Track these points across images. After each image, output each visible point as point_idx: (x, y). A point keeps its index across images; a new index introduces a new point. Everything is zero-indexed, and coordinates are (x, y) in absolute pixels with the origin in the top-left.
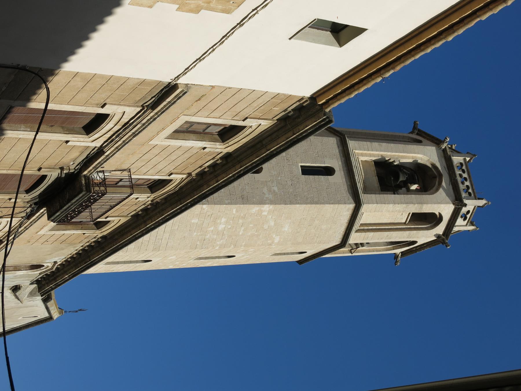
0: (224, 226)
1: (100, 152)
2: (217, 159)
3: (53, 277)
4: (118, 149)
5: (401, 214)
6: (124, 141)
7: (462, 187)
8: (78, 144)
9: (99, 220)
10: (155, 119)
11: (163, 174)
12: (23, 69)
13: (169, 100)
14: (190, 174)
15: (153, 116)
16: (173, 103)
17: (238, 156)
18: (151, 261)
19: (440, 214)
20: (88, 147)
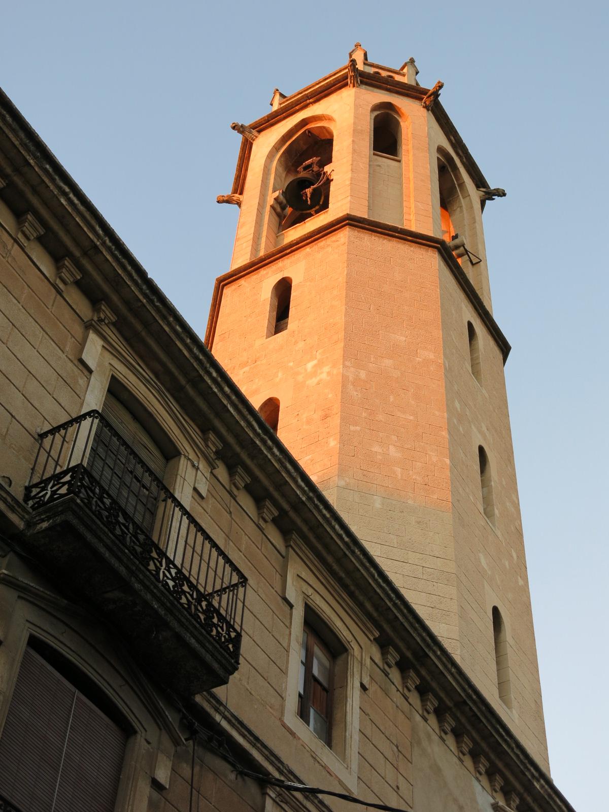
2: (460, 753)
3: (188, 387)
5: (378, 168)
17: (379, 627)
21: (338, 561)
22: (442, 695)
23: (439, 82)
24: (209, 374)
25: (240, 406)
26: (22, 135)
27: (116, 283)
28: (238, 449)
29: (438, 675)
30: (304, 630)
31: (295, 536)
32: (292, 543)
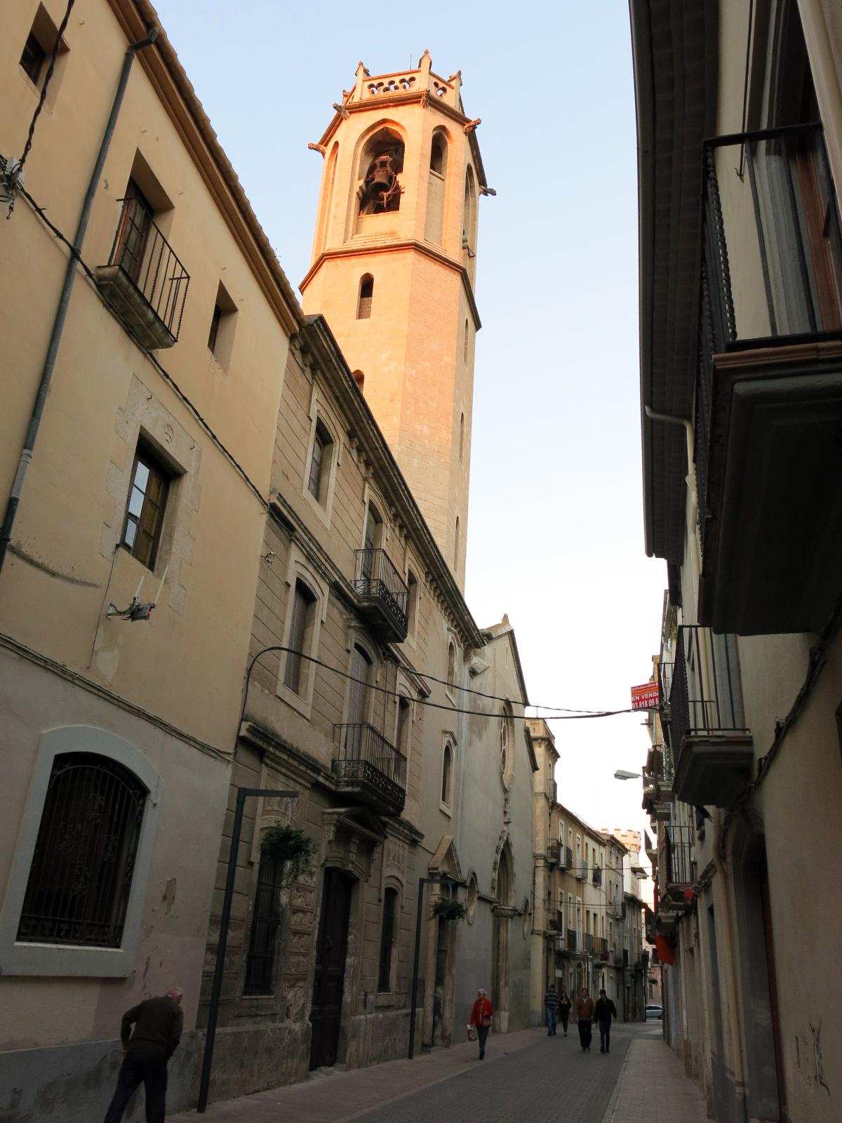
0: (425, 426)
1: (336, 588)
4: (334, 567)
6: (326, 561)
7: (401, 92)
8: (325, 610)
9: (406, 584)
10: (306, 528)
11: (363, 511)
12: (249, 671)
13: (286, 513)
14: (365, 480)
15: (302, 529)
16: (290, 508)
17: (351, 424)
18: (458, 517)
19: (435, 129)
20: (329, 599)
21: (423, 547)
22: (363, 440)
23: (479, 119)
24: (401, 488)
25: (409, 498)
26: (364, 411)
27: (379, 459)
28: (401, 512)
29: (444, 583)
30: (316, 439)
31: (410, 540)
32: (316, 378)
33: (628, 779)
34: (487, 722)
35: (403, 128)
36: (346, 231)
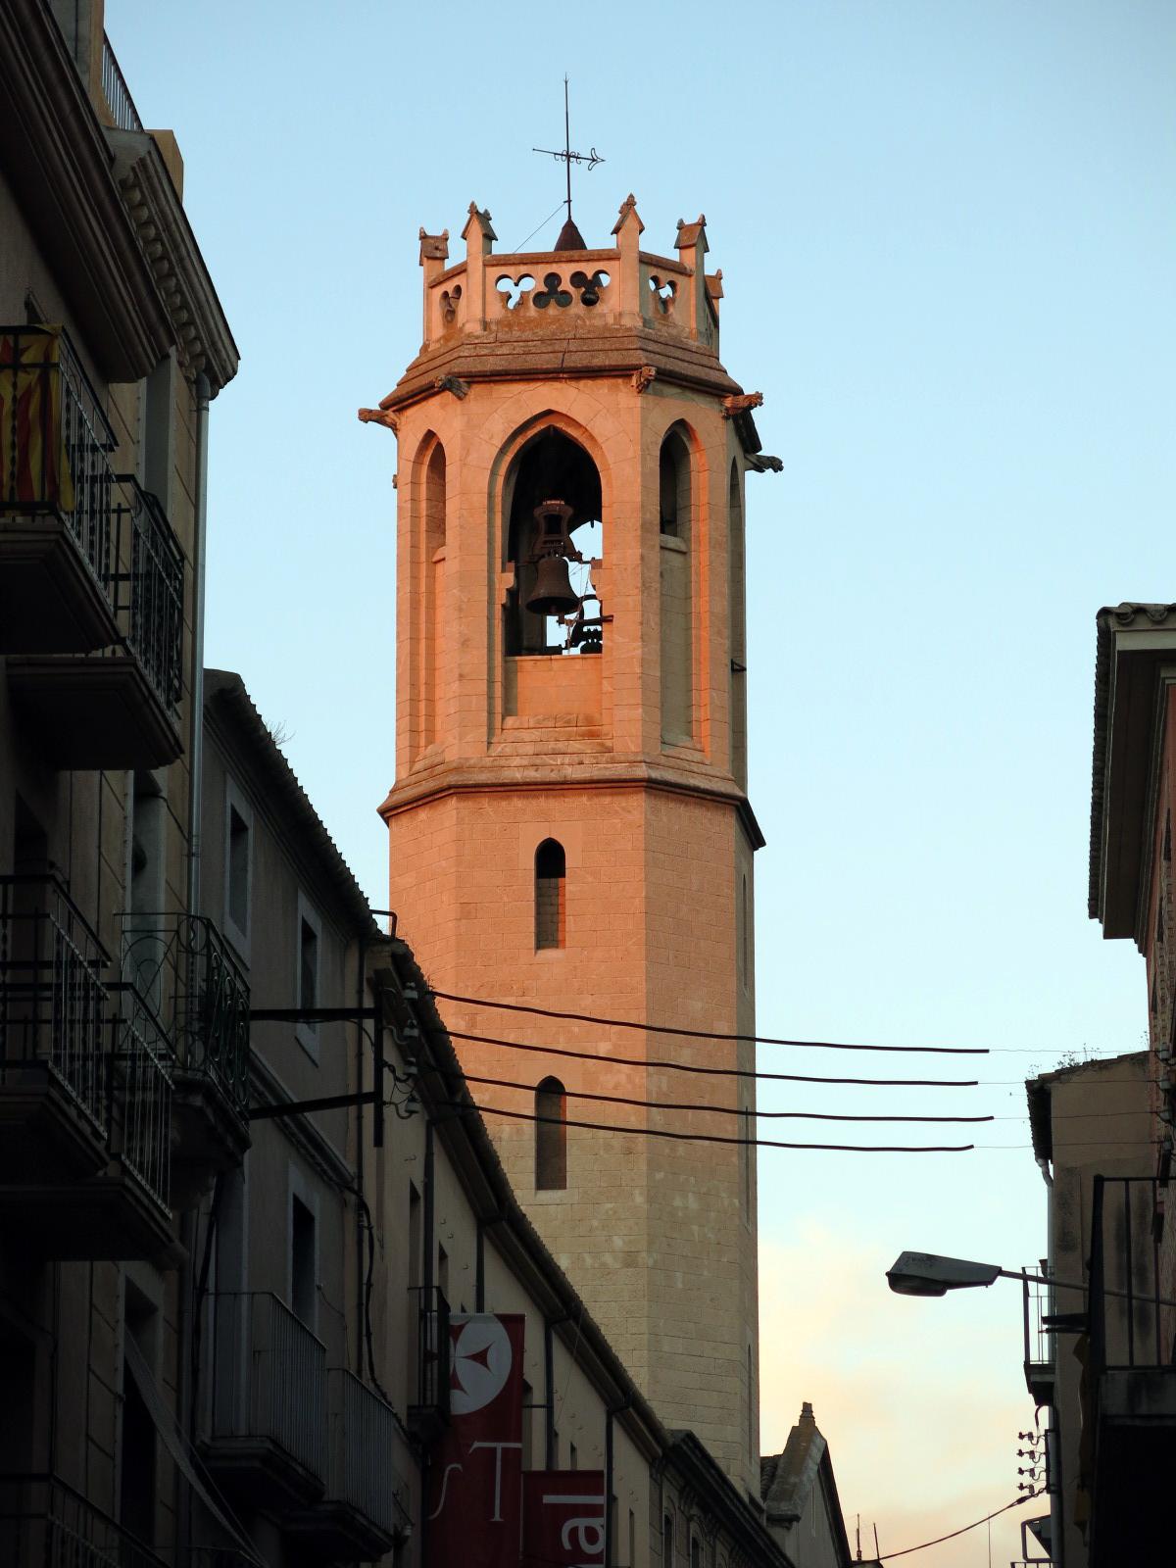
14: (689, 1519)
33: (951, 1294)
34: (649, 1092)
35: (592, 438)
36: (491, 713)
